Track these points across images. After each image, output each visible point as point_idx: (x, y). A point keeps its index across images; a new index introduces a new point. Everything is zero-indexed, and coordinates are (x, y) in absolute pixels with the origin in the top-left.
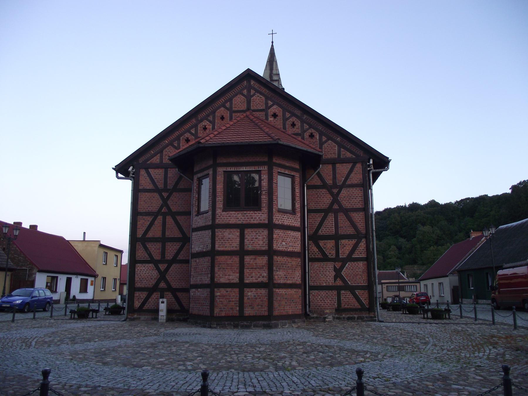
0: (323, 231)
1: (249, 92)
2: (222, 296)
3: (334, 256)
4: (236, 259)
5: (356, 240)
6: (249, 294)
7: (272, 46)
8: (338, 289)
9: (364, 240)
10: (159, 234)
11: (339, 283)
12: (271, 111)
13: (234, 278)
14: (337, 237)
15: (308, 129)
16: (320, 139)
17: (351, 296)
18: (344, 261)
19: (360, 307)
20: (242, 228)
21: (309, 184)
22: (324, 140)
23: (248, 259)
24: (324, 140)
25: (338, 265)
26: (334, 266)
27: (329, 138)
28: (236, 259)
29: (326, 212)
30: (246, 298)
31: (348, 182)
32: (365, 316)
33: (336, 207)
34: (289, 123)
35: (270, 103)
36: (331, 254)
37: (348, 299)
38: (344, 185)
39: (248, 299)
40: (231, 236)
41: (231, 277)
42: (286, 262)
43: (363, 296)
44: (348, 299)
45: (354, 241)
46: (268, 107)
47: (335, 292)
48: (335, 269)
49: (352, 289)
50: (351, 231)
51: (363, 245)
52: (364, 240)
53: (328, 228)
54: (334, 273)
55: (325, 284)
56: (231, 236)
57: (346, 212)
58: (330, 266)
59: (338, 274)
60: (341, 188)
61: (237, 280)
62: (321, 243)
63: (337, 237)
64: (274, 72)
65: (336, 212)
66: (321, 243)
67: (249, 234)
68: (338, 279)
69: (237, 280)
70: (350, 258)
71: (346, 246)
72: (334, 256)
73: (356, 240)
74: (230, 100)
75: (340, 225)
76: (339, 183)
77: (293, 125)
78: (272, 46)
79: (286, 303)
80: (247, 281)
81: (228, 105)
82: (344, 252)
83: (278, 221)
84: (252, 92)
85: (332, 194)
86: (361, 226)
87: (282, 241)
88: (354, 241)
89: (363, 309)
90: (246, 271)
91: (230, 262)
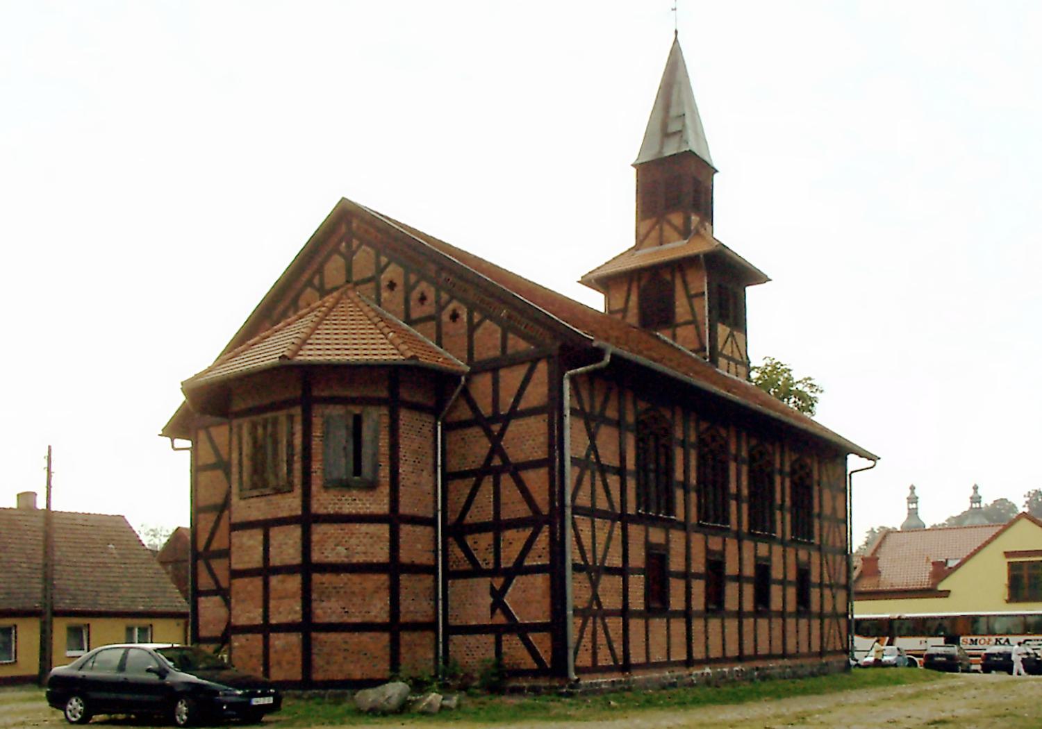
0: (472, 517)
1: (349, 246)
2: (242, 647)
3: (491, 566)
4: (258, 581)
5: (532, 529)
6: (277, 643)
7: (676, 40)
8: (497, 631)
9: (546, 528)
10: (489, 516)
11: (500, 619)
12: (385, 278)
13: (256, 617)
14: (497, 526)
15: (448, 302)
16: (470, 318)
17: (521, 645)
18: (509, 575)
19: (535, 666)
20: (266, 526)
21: (449, 420)
22: (476, 320)
23: (274, 581)
24: (476, 320)
25: (498, 582)
26: (492, 585)
27: (487, 316)
28: (258, 581)
29: (478, 474)
30: (272, 650)
31: (522, 406)
32: (525, 684)
33: (497, 462)
34: (415, 295)
35: (384, 260)
36: (485, 558)
37: (514, 648)
38: (514, 414)
39: (276, 652)
40: (251, 542)
41: (252, 615)
42: (346, 584)
43: (542, 643)
44: (514, 648)
45: (528, 532)
46: (381, 270)
47: (491, 638)
48: (493, 592)
49: (523, 630)
50: (523, 511)
51: (543, 539)
52: (546, 528)
53: (482, 510)
54: (490, 600)
55: (474, 623)
56: (251, 542)
57: (516, 470)
58: (483, 584)
59: (498, 603)
60: (506, 420)
61: (259, 621)
62: (470, 540)
63: (497, 526)
64: (674, 112)
65: (497, 473)
66: (470, 540)
67: (277, 534)
68: (498, 611)
69: (259, 621)
70: (519, 569)
71: (514, 540)
72: (491, 566)
73: (532, 529)
74: (320, 271)
75: (503, 499)
76: (504, 411)
77: (423, 299)
78: (676, 40)
79: (345, 658)
80: (273, 621)
81: (316, 281)
82: (509, 557)
83: (326, 508)
84: (355, 243)
85: (489, 433)
86: (541, 497)
87: (337, 545)
88: (528, 532)
89: (541, 671)
90: (272, 603)
91: (250, 588)
